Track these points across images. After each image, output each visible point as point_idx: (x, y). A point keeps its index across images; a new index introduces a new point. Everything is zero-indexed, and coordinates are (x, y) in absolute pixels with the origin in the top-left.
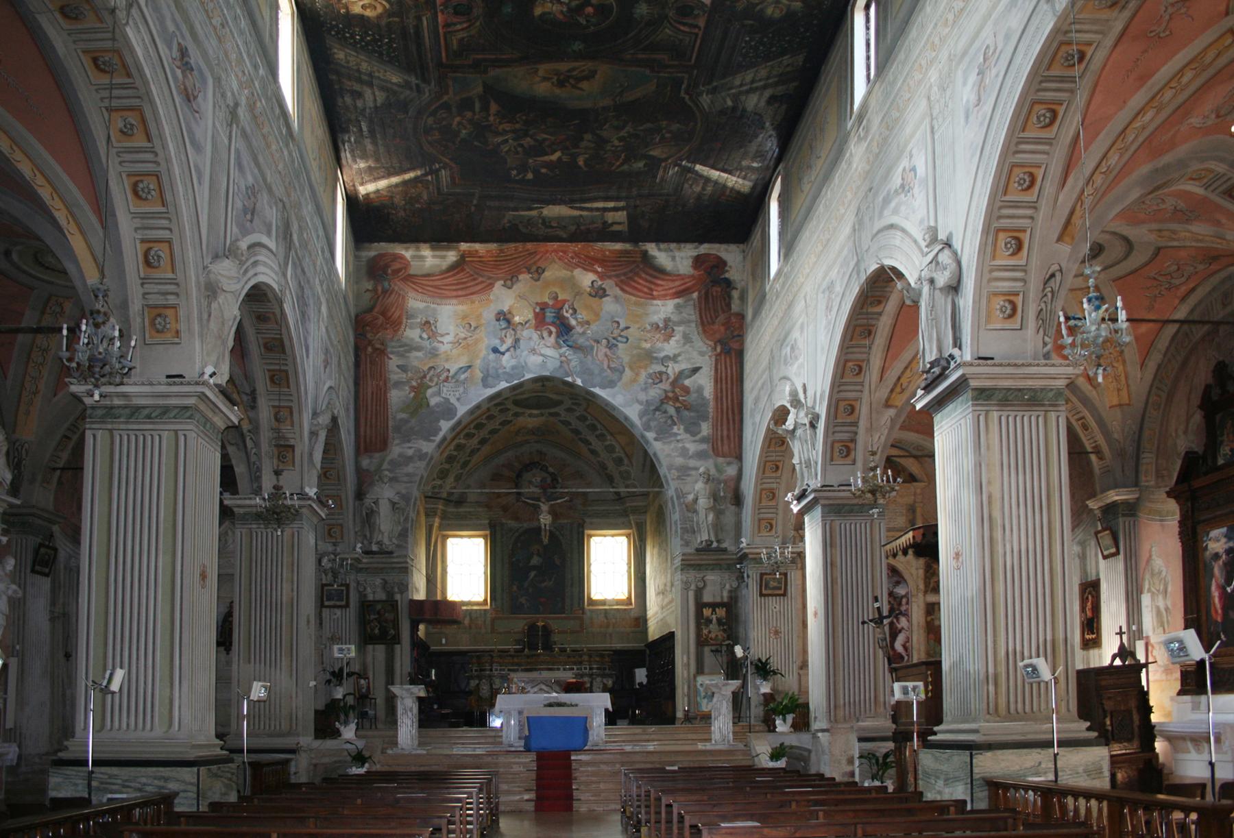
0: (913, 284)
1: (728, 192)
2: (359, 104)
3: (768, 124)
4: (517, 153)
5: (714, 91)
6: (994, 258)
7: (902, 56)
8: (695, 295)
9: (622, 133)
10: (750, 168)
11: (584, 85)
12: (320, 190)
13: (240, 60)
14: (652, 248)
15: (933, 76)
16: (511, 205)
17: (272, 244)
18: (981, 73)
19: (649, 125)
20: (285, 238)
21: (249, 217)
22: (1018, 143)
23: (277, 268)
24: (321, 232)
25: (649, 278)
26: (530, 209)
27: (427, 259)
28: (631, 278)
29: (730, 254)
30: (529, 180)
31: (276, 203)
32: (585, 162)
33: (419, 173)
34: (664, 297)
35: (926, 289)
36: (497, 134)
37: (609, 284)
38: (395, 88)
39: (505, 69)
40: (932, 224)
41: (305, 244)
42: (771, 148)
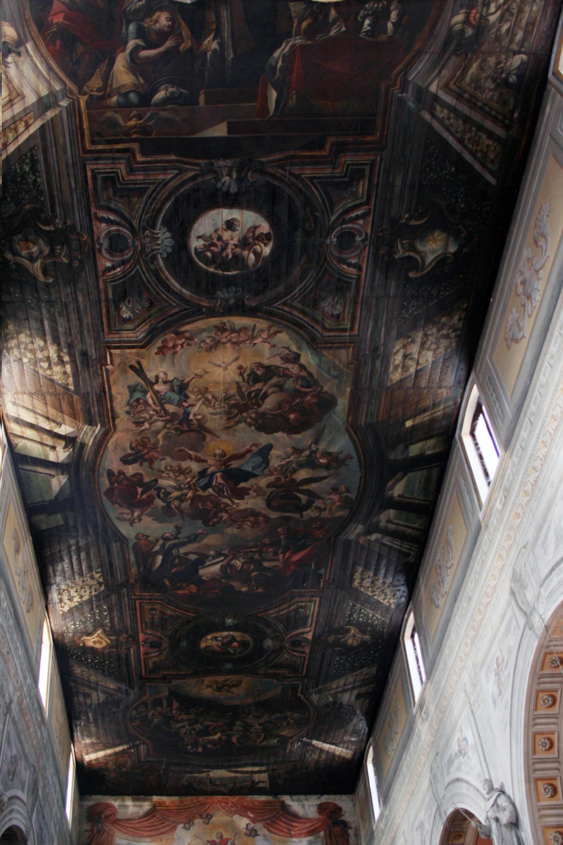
0: (483, 822)
1: (337, 759)
2: (88, 701)
3: (358, 712)
4: (192, 734)
5: (320, 692)
6: (539, 800)
7: (441, 666)
8: (322, 833)
9: (262, 721)
10: (349, 741)
11: (234, 690)
12: (59, 758)
13: (16, 674)
14: (287, 799)
15: (465, 677)
16: (188, 769)
17: (24, 796)
18: (497, 674)
19: (278, 715)
20: (33, 792)
21: (11, 777)
22: (534, 719)
23: (25, 814)
24: (58, 788)
25: (287, 821)
26: (201, 772)
27: (130, 807)
28: (273, 822)
29: (343, 802)
30: (200, 753)
31: (30, 767)
32: (238, 739)
33: (125, 747)
34: (299, 835)
35: (494, 826)
36: (178, 722)
37: (259, 826)
38: (112, 692)
39: (183, 681)
40: (487, 777)
41: (46, 797)
42: (363, 728)
